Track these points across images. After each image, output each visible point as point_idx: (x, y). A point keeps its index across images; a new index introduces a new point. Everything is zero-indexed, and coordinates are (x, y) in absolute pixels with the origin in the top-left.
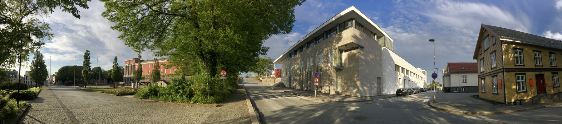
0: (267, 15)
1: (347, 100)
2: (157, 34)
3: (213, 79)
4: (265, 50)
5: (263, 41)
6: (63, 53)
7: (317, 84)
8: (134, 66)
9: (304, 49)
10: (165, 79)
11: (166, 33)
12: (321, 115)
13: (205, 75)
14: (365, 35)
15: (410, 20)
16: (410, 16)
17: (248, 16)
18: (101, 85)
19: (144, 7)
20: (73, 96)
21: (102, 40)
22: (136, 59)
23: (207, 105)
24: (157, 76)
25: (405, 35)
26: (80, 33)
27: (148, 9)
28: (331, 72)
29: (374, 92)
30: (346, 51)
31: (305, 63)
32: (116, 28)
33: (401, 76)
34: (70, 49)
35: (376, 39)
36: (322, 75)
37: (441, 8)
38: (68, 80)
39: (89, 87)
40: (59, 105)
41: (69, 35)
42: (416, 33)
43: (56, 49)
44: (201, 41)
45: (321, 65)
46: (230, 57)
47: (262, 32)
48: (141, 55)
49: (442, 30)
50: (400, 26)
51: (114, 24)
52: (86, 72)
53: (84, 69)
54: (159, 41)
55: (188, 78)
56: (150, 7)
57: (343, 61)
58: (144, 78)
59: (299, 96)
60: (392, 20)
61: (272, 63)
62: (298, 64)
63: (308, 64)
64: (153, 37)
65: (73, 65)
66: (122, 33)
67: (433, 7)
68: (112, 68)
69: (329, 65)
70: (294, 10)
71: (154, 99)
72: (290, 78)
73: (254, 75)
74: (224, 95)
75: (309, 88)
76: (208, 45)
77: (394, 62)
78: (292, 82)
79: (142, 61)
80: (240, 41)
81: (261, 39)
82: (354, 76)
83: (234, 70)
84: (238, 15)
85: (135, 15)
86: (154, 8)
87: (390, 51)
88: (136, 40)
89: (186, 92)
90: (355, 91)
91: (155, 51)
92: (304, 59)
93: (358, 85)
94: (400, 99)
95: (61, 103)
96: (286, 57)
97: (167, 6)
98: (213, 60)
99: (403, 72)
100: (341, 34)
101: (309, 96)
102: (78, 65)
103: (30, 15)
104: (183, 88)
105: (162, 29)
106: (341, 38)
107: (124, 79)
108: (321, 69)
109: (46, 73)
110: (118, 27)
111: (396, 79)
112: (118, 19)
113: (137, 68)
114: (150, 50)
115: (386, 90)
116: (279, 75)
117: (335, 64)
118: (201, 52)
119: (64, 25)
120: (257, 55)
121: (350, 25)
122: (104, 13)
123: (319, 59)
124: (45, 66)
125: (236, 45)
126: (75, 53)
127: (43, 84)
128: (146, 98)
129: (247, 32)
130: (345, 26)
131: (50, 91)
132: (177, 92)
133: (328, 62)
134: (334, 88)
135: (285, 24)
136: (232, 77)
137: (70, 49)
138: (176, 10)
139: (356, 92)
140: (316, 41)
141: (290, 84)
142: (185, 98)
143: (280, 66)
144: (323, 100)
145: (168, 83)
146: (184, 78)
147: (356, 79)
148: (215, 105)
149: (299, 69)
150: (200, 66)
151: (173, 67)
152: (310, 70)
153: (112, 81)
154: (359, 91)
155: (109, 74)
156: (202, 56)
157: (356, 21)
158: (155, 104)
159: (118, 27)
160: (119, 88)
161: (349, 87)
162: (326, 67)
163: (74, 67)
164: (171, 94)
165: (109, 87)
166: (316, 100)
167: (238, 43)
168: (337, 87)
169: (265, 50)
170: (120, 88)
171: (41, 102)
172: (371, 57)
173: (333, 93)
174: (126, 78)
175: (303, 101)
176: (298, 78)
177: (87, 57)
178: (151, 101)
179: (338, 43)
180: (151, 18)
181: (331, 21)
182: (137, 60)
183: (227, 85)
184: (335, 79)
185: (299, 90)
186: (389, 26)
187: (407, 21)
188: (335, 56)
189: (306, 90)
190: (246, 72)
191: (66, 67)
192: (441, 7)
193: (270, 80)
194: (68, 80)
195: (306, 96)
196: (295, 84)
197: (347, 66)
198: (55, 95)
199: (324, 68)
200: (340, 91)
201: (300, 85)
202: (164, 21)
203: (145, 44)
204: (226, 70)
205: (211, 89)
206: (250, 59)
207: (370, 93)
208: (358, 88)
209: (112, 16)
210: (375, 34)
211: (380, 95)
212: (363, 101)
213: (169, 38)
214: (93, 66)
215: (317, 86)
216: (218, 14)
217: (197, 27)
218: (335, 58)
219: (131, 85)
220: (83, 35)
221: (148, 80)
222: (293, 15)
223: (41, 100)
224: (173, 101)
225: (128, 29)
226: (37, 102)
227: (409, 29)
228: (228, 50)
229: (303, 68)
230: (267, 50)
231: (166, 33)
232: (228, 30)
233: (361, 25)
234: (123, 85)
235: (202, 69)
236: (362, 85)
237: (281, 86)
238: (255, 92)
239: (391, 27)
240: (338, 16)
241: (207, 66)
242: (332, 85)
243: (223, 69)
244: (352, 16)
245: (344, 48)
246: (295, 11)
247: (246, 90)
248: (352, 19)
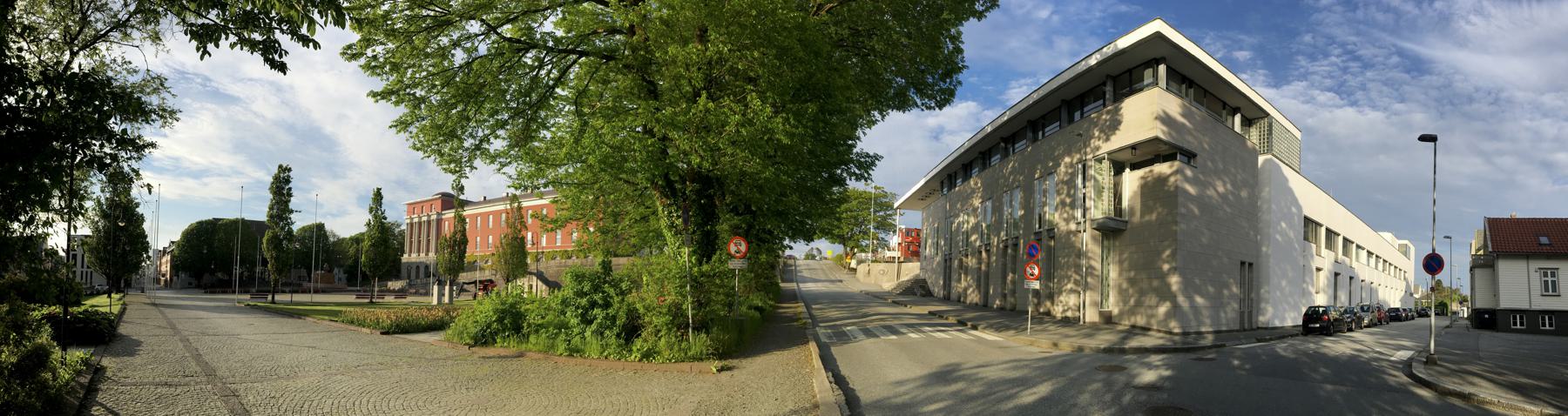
0: (873, 49)
1: (1134, 343)
2: (517, 113)
3: (705, 268)
4: (867, 164)
5: (859, 132)
6: (198, 174)
7: (1036, 285)
8: (439, 222)
9: (996, 159)
10: (542, 266)
11: (550, 108)
12: (1043, 401)
13: (679, 254)
14: (1199, 112)
15: (1367, 66)
16: (1366, 52)
17: (817, 54)
18: (324, 291)
19: (474, 27)
20: (231, 329)
21: (329, 129)
22: (444, 195)
23: (686, 366)
24: (516, 258)
25: (1350, 112)
26: (258, 106)
27: (486, 34)
28: (1087, 240)
29: (1230, 315)
30: (1134, 167)
31: (997, 210)
32: (384, 95)
33: (1324, 259)
34: (225, 161)
35: (1238, 128)
36: (1051, 251)
37: (1468, 27)
38: (213, 273)
39: (286, 297)
40: (193, 366)
41: (222, 112)
42: (1385, 109)
43: (177, 159)
44: (664, 138)
45: (1054, 216)
46: (761, 189)
47: (858, 101)
48: (463, 181)
49: (1471, 100)
50: (1328, 82)
51: (379, 84)
52: (276, 242)
53: (268, 235)
54: (522, 140)
55: (621, 264)
56: (491, 29)
57: (1125, 204)
58: (473, 267)
59: (975, 328)
60: (1303, 61)
61: (889, 206)
62: (975, 210)
63: (1007, 211)
64: (503, 124)
65: (230, 214)
66: (402, 110)
67: (1444, 24)
68: (364, 229)
69: (1079, 214)
70: (960, 33)
71: (512, 346)
72: (947, 260)
73: (827, 248)
74: (740, 326)
75: (1010, 300)
76: (688, 152)
77: (1299, 208)
78: (954, 276)
79: (464, 204)
80: (791, 136)
81: (854, 127)
82: (1159, 253)
83: (770, 232)
84: (783, 53)
85: (444, 53)
86: (507, 30)
87: (1286, 170)
88: (452, 135)
89: (614, 318)
90: (1163, 309)
91: (511, 170)
92: (993, 193)
93: (1175, 288)
94: (1311, 344)
95: (198, 357)
96: (937, 185)
97: (550, 26)
98: (704, 201)
99: (1330, 244)
100: (1117, 110)
101: (1008, 328)
102: (248, 217)
103: (102, 46)
104: (607, 305)
105: (534, 96)
106: (1120, 123)
107: (404, 271)
108: (1051, 230)
109: (139, 241)
110: (391, 93)
111: (1305, 272)
112: (395, 67)
113: (447, 229)
114: (496, 166)
115: (1270, 311)
116: (913, 250)
117: (1099, 209)
118: (666, 177)
119: (207, 79)
120: (841, 182)
121: (1148, 79)
122: (350, 47)
123: (1045, 192)
124: (141, 219)
125: (779, 146)
126: (238, 173)
127: (128, 285)
128: (485, 344)
129: (812, 108)
130: (1131, 83)
131: (154, 311)
132: (586, 321)
133: (1073, 206)
134: (1095, 296)
135: (934, 79)
136: (763, 258)
137: (225, 161)
138: (583, 38)
139: (1168, 315)
140: (1035, 132)
141: (947, 285)
142: (613, 340)
143: (909, 219)
144: (1055, 345)
145: (553, 285)
146: (607, 267)
147: (1166, 267)
148: (714, 365)
149: (976, 228)
150: (664, 222)
151: (572, 226)
152: (1014, 233)
153: (364, 275)
154: (1176, 310)
155: (352, 251)
156: (669, 190)
157: (1170, 70)
158: (515, 363)
159: (391, 93)
160: (388, 306)
161: (1142, 293)
162: (1067, 221)
163: (236, 222)
164: (564, 326)
165: (351, 298)
166: (1032, 345)
167: (786, 141)
168: (1104, 296)
169: (867, 164)
170: (393, 304)
171: (132, 354)
172: (1221, 189)
173: (1091, 316)
174: (409, 265)
175: (990, 349)
176: (971, 262)
177: (281, 187)
178: (503, 352)
179: (1107, 139)
180: (496, 64)
181: (1082, 67)
182: (448, 201)
183: (748, 289)
184: (1098, 265)
185: (974, 307)
186: (1289, 83)
187: (1354, 66)
188: (1092, 190)
189: (1001, 309)
190: (809, 239)
191: (208, 223)
192: (1468, 22)
193: (882, 272)
194: (213, 273)
195: (998, 328)
196: (964, 284)
197: (1137, 218)
198: (173, 327)
199: (1063, 226)
200: (1116, 311)
201: (978, 287)
202: (543, 72)
203: (478, 147)
204: (746, 236)
205: (699, 305)
206: (817, 194)
207: (1215, 319)
208: (1172, 297)
209: (375, 57)
210: (1235, 111)
211: (1249, 328)
212: (1188, 350)
213: (559, 123)
214: (299, 222)
215: (1036, 293)
216: (720, 53)
217: (653, 92)
218: (1099, 191)
219: (427, 294)
220: (270, 113)
221: (487, 275)
222: (960, 51)
223: (130, 347)
224: (573, 351)
225: (423, 100)
226: (117, 355)
227: (1359, 95)
228: (753, 165)
229: (988, 227)
230: (873, 164)
231: (550, 108)
232: (756, 103)
233: (1189, 79)
234: (401, 293)
235: (668, 235)
236: (1189, 288)
237: (917, 290)
238: (834, 314)
239: (1299, 86)
240: (1109, 50)
241: (685, 222)
242: (1086, 287)
243: (735, 231)
244: (1156, 53)
245: (1126, 156)
246: (963, 38)
247: (808, 307)
248: (1157, 62)
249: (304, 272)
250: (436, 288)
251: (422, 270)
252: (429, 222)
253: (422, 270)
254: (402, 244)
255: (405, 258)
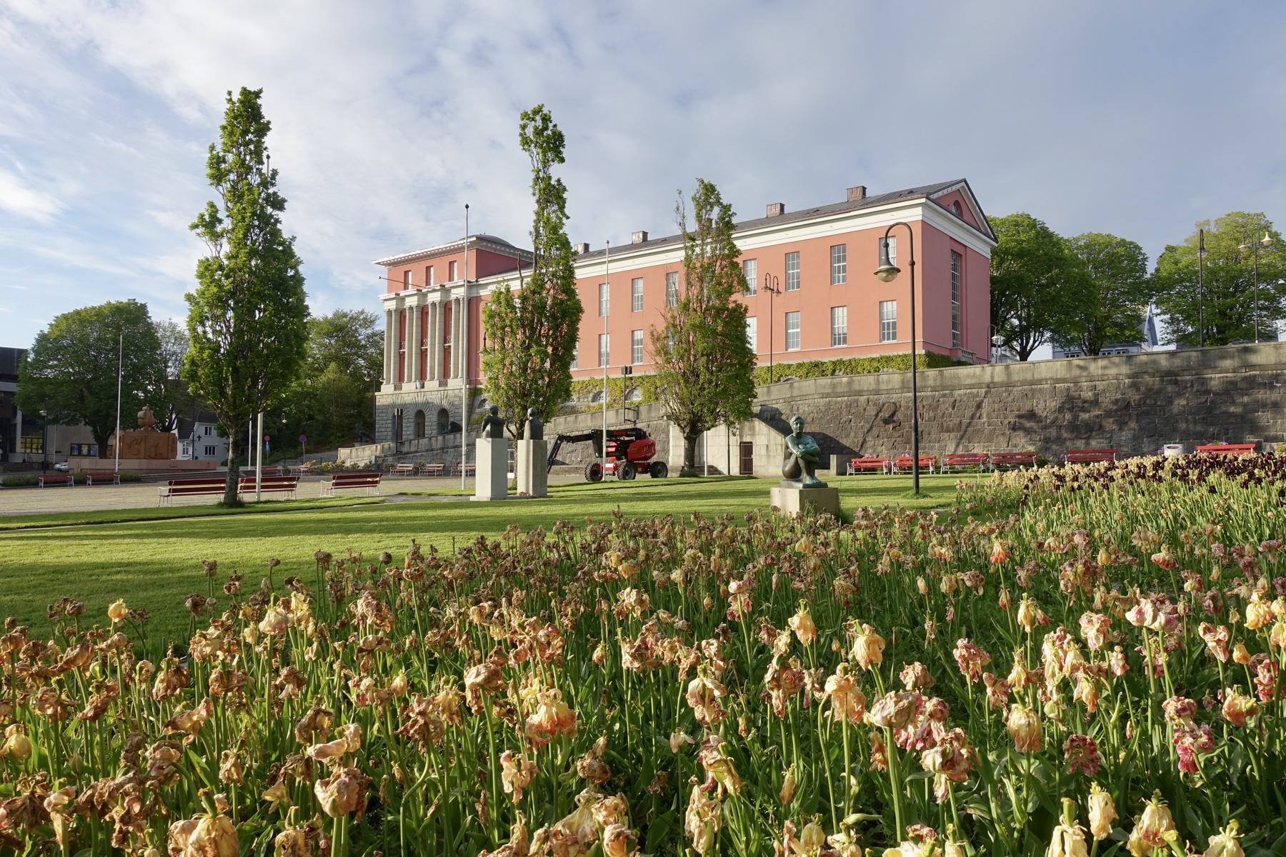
8: (473, 302)
107: (383, 425)
249: (85, 433)
250: (484, 447)
251: (431, 419)
252: (446, 307)
253: (431, 419)
254: (377, 366)
255: (386, 395)
